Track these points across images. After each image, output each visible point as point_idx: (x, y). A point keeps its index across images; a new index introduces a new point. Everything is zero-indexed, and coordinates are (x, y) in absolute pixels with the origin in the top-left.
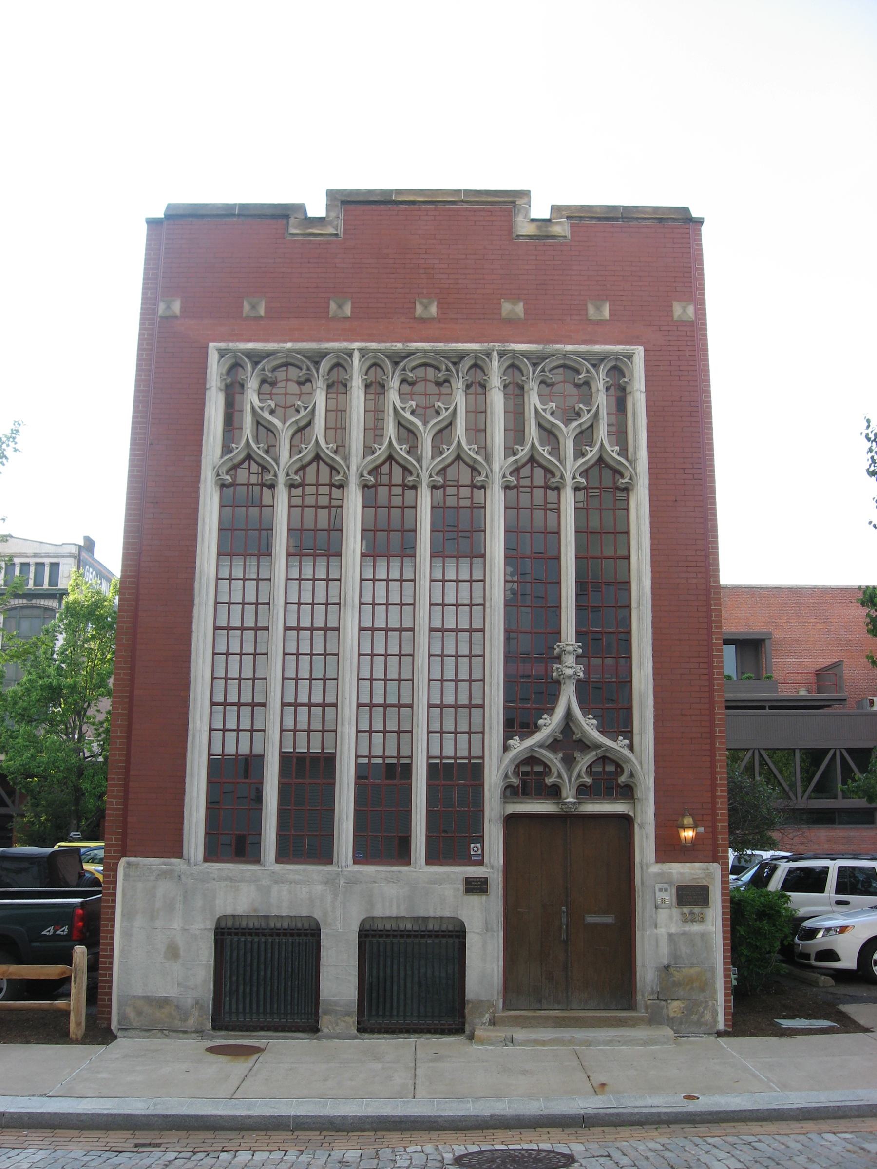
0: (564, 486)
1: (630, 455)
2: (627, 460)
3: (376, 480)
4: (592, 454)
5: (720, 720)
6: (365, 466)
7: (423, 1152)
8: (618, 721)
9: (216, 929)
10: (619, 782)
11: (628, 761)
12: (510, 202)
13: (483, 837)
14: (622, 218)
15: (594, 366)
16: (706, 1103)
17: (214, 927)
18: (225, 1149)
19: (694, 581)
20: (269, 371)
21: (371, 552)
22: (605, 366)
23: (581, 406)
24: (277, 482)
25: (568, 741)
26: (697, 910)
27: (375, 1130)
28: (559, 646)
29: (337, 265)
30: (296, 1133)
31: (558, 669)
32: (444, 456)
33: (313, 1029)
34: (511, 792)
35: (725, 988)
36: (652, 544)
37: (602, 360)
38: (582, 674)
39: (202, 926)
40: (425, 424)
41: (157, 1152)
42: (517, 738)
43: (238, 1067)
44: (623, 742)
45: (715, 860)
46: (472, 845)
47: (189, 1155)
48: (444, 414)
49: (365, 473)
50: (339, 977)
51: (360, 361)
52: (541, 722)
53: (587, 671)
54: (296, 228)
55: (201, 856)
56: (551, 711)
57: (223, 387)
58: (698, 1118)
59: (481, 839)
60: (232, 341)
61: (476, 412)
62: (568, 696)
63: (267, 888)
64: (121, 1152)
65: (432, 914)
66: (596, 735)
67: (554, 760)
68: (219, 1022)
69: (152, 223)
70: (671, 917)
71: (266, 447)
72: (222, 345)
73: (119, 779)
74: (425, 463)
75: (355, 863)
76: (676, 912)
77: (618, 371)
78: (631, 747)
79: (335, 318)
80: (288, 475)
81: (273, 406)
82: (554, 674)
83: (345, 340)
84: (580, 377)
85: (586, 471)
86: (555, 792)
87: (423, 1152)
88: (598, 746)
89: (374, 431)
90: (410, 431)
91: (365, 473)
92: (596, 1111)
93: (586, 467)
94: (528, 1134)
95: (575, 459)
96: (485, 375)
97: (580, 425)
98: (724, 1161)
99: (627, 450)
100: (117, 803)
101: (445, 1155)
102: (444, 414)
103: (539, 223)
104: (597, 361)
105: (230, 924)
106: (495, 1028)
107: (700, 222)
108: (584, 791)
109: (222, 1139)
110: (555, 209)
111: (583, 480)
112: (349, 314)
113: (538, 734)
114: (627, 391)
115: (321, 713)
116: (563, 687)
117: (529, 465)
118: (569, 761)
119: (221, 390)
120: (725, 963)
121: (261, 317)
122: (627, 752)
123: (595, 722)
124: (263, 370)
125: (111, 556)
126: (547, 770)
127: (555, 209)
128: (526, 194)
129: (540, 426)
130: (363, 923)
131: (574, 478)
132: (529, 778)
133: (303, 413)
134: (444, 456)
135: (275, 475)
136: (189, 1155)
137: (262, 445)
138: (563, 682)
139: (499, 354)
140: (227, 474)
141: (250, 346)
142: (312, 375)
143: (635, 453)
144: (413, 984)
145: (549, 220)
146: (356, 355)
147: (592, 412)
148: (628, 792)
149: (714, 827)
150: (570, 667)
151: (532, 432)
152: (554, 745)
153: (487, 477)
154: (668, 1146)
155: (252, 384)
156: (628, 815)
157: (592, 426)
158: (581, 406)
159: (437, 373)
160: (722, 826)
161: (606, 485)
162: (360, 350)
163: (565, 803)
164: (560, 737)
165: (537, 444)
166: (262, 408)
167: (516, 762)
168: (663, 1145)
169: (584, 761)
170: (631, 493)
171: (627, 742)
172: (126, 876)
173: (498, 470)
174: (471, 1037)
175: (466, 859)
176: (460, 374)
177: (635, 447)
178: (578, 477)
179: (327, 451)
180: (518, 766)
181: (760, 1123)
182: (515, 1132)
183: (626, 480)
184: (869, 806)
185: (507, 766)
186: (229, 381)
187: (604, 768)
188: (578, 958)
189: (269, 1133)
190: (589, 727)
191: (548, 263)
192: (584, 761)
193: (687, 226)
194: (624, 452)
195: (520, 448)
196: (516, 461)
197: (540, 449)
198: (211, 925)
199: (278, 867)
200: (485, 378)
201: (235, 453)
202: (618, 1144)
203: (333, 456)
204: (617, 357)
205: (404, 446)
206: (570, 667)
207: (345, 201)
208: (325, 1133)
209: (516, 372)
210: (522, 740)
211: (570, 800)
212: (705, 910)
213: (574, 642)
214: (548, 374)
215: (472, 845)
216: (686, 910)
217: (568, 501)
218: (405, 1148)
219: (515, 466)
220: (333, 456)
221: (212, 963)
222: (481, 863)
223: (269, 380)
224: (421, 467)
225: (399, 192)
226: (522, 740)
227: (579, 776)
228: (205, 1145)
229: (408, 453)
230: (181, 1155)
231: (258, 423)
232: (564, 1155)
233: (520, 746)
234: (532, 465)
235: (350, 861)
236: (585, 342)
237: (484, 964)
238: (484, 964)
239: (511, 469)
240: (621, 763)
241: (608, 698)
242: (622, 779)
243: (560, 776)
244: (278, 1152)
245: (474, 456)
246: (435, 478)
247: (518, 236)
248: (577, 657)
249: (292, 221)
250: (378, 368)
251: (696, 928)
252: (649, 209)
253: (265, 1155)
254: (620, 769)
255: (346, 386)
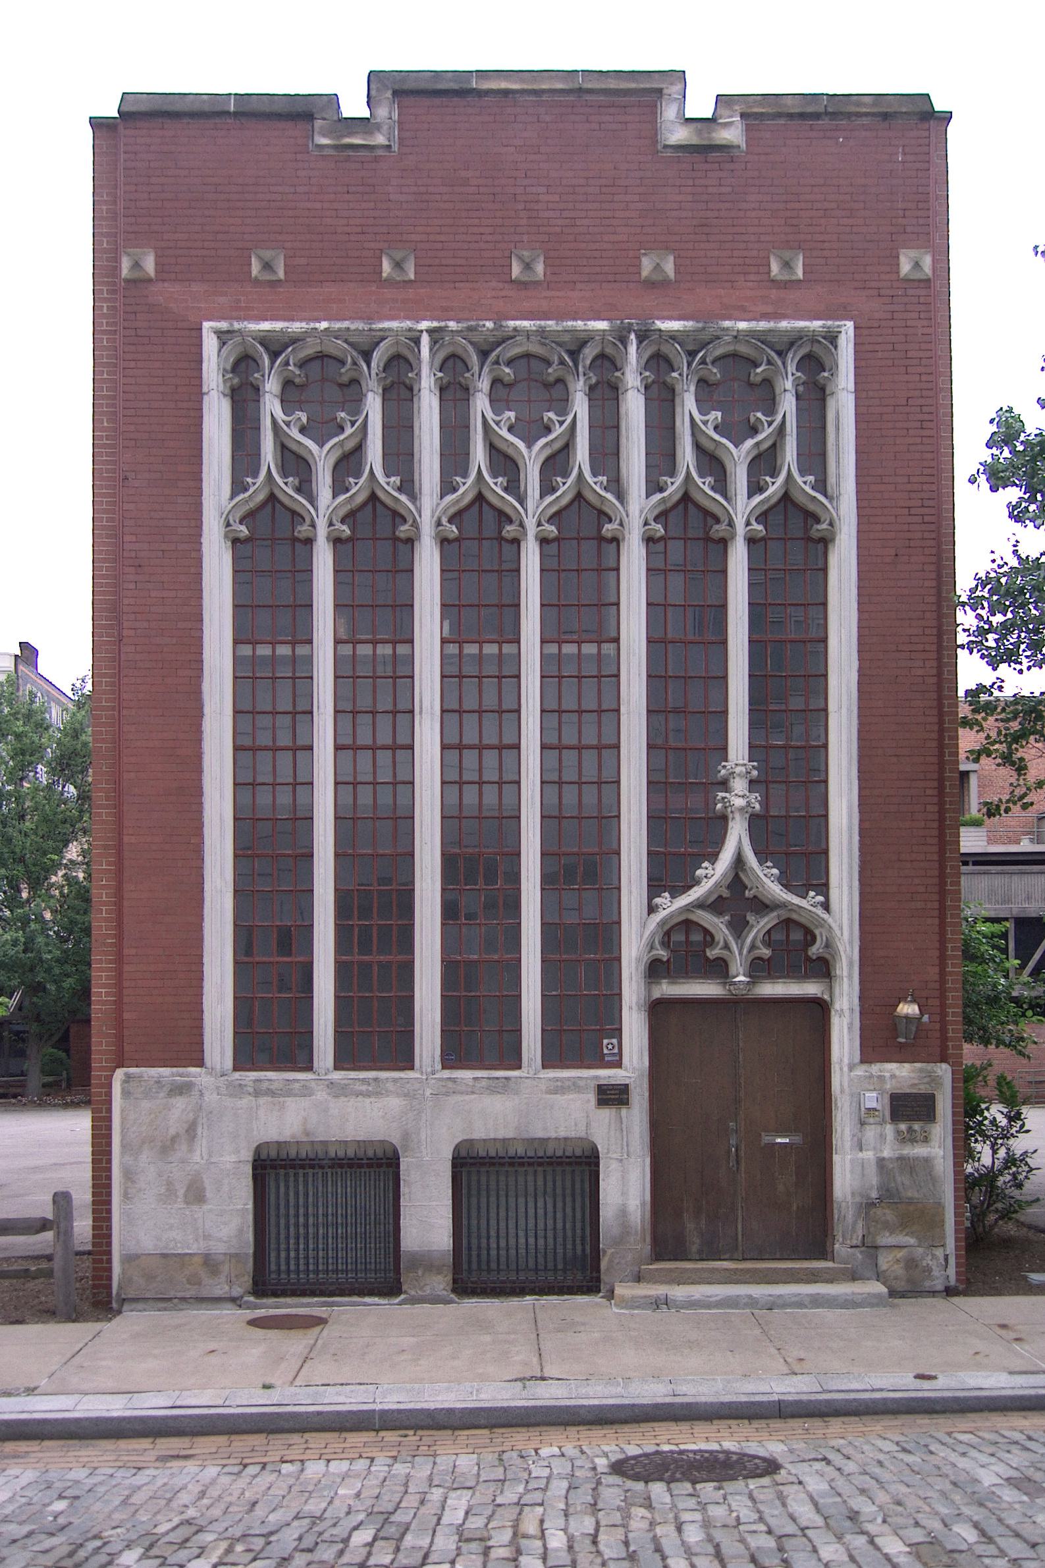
0: (733, 536)
1: (829, 489)
2: (826, 496)
3: (353, 530)
4: (774, 488)
5: (951, 803)
6: (445, 511)
7: (563, 1455)
8: (808, 870)
9: (255, 1160)
10: (810, 953)
11: (822, 923)
12: (647, 92)
13: (620, 1030)
14: (826, 113)
15: (780, 353)
16: (947, 1384)
17: (251, 1159)
18: (285, 1458)
19: (920, 672)
20: (295, 365)
21: (455, 637)
22: (795, 352)
23: (759, 415)
24: (316, 535)
25: (736, 899)
26: (916, 1126)
27: (491, 1427)
28: (724, 767)
29: (392, 197)
30: (382, 1434)
31: (723, 798)
32: (558, 494)
33: (390, 1288)
34: (655, 970)
35: (956, 1231)
36: (860, 620)
37: (792, 344)
38: (757, 806)
39: (234, 1158)
40: (529, 447)
41: (191, 1467)
42: (666, 894)
43: (295, 1343)
44: (815, 898)
45: (943, 1059)
46: (605, 1041)
47: (236, 1469)
48: (558, 430)
49: (444, 520)
50: (427, 1219)
51: (431, 350)
52: (699, 872)
53: (766, 802)
54: (324, 136)
55: (229, 1063)
56: (713, 858)
57: (228, 391)
58: (938, 1408)
59: (618, 1032)
60: (239, 319)
61: (605, 428)
62: (737, 835)
63: (328, 1106)
64: (139, 1469)
65: (553, 1135)
66: (776, 891)
67: (718, 925)
68: (264, 1285)
69: (98, 124)
70: (882, 1137)
71: (297, 482)
72: (223, 325)
73: (110, 962)
74: (531, 504)
75: (444, 1068)
76: (889, 1129)
77: (815, 365)
78: (826, 906)
79: (390, 282)
80: (331, 524)
81: (304, 420)
82: (719, 806)
83: (408, 318)
84: (759, 370)
85: (557, 514)
86: (719, 969)
87: (563, 1455)
88: (784, 905)
89: (454, 457)
90: (300, 458)
91: (444, 520)
92: (796, 1397)
93: (765, 507)
94: (701, 1428)
95: (750, 496)
96: (617, 370)
97: (757, 444)
98: (992, 1467)
99: (825, 481)
100: (108, 978)
101: (597, 1460)
102: (558, 430)
103: (699, 125)
104: (784, 346)
105: (273, 1154)
106: (641, 1285)
107: (947, 117)
108: (760, 969)
109: (277, 1445)
110: (722, 100)
111: (760, 528)
112: (412, 277)
113: (695, 889)
114: (828, 392)
115: (563, 701)
116: (731, 824)
117: (477, 504)
118: (739, 927)
119: (225, 395)
120: (956, 1198)
121: (280, 281)
122: (820, 911)
123: (775, 871)
124: (287, 364)
125: (69, 663)
126: (708, 938)
127: (722, 100)
128: (679, 76)
129: (698, 447)
130: (457, 1148)
131: (748, 524)
132: (683, 949)
133: (349, 431)
134: (558, 494)
135: (313, 525)
136: (236, 1469)
137: (291, 479)
138: (731, 816)
139: (637, 337)
140: (241, 523)
141: (266, 326)
142: (361, 373)
143: (838, 484)
144: (528, 1232)
145: (712, 120)
146: (425, 340)
147: (775, 424)
148: (823, 969)
149: (943, 1014)
150: (739, 797)
151: (687, 456)
152: (715, 905)
153: (621, 524)
154: (905, 1445)
155: (271, 386)
156: (825, 1001)
157: (774, 445)
158: (759, 415)
159: (533, 384)
160: (954, 1012)
161: (794, 533)
162: (430, 331)
163: (735, 983)
164: (726, 893)
165: (694, 474)
166: (288, 424)
167: (666, 928)
168: (897, 1443)
169: (760, 925)
170: (830, 546)
171: (821, 898)
172: (126, 1094)
173: (637, 513)
174: (611, 1295)
175: (601, 1062)
176: (581, 369)
177: (838, 476)
178: (753, 522)
179: (386, 487)
180: (668, 934)
181: (1023, 1413)
182: (685, 1427)
183: (616, 526)
184: (970, 447)
185: (653, 935)
186: (236, 381)
187: (788, 936)
188: (747, 1195)
189: (344, 1435)
190: (767, 880)
191: (710, 190)
192: (760, 925)
193: (926, 125)
194: (821, 485)
195: (669, 480)
196: (663, 500)
197: (699, 481)
198: (248, 1155)
199: (338, 1075)
200: (618, 374)
201: (251, 490)
202: (834, 1443)
203: (396, 494)
204: (812, 338)
205: (500, 479)
206: (739, 797)
207: (409, 93)
208: (420, 1432)
209: (607, 364)
210: (673, 897)
211: (741, 978)
212: (928, 1127)
213: (746, 762)
214: (710, 367)
215: (605, 1041)
216: (903, 1127)
217: (738, 560)
218: (536, 1451)
219: (662, 508)
220: (396, 494)
221: (250, 1206)
222: (618, 1064)
223: (297, 380)
224: (526, 511)
225: (482, 74)
226: (673, 897)
227: (753, 947)
228: (254, 1454)
229: (506, 490)
230: (226, 1470)
231: (493, 449)
232: (764, 1459)
233: (670, 906)
234: (481, 507)
235: (438, 1066)
236: (765, 316)
237: (625, 1189)
238: (625, 1189)
239: (656, 512)
240: (812, 927)
241: (794, 841)
242: (815, 950)
243: (727, 947)
244: (362, 1461)
245: (603, 493)
246: (338, 526)
247: (666, 146)
248: (751, 782)
249: (318, 123)
250: (457, 360)
251: (919, 1151)
252: (866, 99)
253: (344, 1466)
254: (810, 937)
255: (411, 389)
